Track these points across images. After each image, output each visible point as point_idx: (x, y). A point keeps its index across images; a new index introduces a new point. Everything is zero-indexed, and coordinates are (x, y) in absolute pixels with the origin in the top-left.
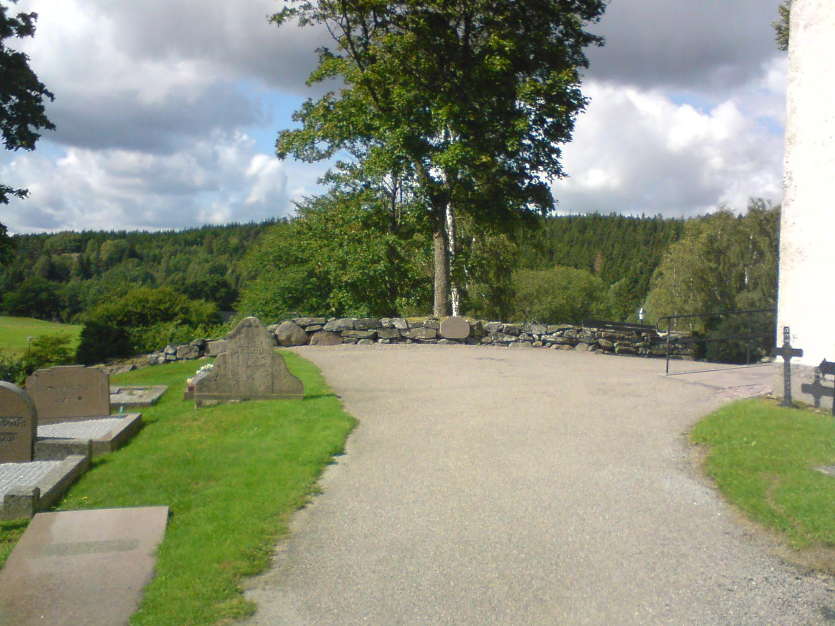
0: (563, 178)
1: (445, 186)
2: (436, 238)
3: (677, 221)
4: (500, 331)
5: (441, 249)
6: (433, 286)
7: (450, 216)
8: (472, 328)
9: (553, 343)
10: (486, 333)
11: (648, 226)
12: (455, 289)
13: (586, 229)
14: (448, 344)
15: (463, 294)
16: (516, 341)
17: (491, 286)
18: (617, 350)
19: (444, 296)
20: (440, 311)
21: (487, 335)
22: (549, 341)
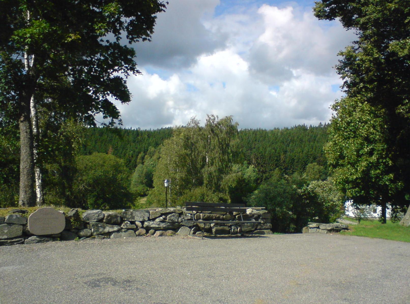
0: (137, 74)
1: (26, 114)
2: (22, 122)
3: (148, 131)
4: (101, 221)
5: (26, 132)
6: (19, 167)
7: (33, 109)
8: (68, 219)
9: (156, 229)
10: (85, 225)
11: (135, 133)
12: (38, 170)
13: (103, 134)
14: (39, 242)
15: (43, 171)
16: (118, 231)
17: (60, 166)
18: (214, 230)
19: (29, 177)
20: (26, 192)
21: (86, 227)
22: (153, 228)
